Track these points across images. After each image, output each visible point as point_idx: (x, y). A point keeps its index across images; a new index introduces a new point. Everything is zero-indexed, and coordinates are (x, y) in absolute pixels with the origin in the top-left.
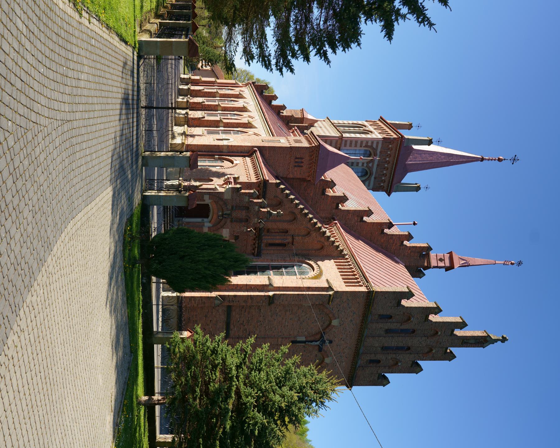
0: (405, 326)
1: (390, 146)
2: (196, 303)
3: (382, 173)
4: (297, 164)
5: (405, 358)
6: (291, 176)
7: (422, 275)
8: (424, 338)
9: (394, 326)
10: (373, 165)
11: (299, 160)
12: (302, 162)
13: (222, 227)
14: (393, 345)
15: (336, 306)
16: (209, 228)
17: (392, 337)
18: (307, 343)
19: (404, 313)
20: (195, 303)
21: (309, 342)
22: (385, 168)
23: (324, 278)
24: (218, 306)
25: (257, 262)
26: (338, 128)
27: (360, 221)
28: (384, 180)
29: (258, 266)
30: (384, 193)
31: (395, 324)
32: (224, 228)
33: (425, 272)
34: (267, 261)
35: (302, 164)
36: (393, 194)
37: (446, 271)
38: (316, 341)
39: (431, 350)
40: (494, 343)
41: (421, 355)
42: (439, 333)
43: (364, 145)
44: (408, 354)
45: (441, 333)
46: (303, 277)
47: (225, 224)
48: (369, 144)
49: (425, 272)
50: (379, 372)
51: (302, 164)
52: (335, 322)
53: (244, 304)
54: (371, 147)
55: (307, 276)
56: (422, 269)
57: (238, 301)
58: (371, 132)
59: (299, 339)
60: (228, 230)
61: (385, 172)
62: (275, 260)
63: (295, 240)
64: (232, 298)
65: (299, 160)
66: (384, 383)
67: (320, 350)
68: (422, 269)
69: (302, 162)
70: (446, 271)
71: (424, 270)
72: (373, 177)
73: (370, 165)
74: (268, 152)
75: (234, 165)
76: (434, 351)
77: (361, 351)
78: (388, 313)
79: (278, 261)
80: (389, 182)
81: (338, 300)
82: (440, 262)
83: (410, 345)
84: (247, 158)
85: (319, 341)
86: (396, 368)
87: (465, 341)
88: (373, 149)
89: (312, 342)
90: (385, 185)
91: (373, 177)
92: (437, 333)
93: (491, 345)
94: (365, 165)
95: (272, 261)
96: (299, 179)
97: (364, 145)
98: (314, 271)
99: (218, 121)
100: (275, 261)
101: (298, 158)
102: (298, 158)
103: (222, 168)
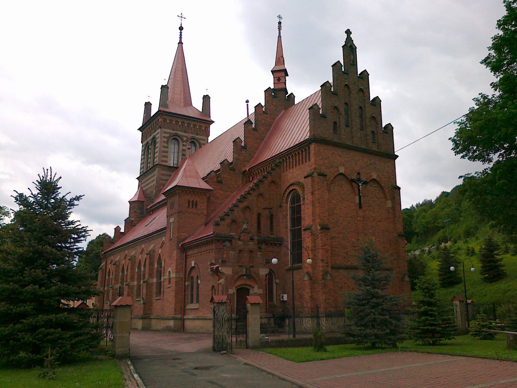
0: (342, 109)
1: (168, 121)
2: (331, 297)
3: (193, 128)
4: (194, 206)
5: (369, 111)
6: (205, 212)
7: (292, 96)
8: (351, 95)
9: (343, 122)
10: (185, 136)
11: (191, 204)
12: (193, 201)
13: (258, 275)
14: (358, 121)
15: (328, 170)
16: (259, 288)
17: (351, 121)
18: (361, 194)
19: (331, 112)
20: (330, 299)
21: (359, 193)
22: (200, 128)
23: (302, 180)
24: (332, 276)
25: (287, 241)
26: (148, 169)
27: (246, 148)
28: (199, 127)
29: (292, 240)
30: (211, 126)
31: (341, 119)
32: (259, 274)
33: (289, 93)
34: (287, 232)
35: (195, 202)
36: (212, 118)
37: (288, 76)
38: (359, 186)
39: (361, 90)
40: (353, 41)
41: (366, 98)
42: (347, 83)
43: (166, 145)
44: (365, 108)
45: (346, 82)
46: (302, 199)
47: (255, 273)
48: (166, 140)
49: (289, 93)
50: (381, 132)
51: (195, 202)
52: (342, 170)
53: (330, 252)
54: (168, 138)
55: (301, 195)
56: (287, 96)
57: (327, 257)
58: (154, 138)
59: (357, 201)
60: (260, 269)
61: (192, 126)
62: (286, 224)
63: (267, 207)
64: (325, 263)
65: (191, 204)
66: (391, 128)
67: (365, 183)
68: (287, 96)
69: (193, 201)
70: (288, 76)
71: (288, 93)
72: (196, 136)
73: (185, 139)
74: (183, 234)
75: (196, 267)
76: (362, 88)
77: (365, 147)
78: (332, 125)
79: (286, 222)
80: (184, 118)
81: (322, 168)
82: (280, 81)
83: (358, 107)
84: (188, 254)
85: (358, 184)
86: (377, 117)
87: (352, 62)
88: (170, 137)
89: (359, 190)
90: (203, 125)
91: (196, 136)
92: (346, 85)
93: (354, 42)
94: (185, 143)
95: (287, 227)
96: (208, 203)
97: (166, 145)
98: (295, 189)
99: (147, 285)
100: (287, 224)
101: (189, 205)
102: (189, 205)
103: (199, 277)
